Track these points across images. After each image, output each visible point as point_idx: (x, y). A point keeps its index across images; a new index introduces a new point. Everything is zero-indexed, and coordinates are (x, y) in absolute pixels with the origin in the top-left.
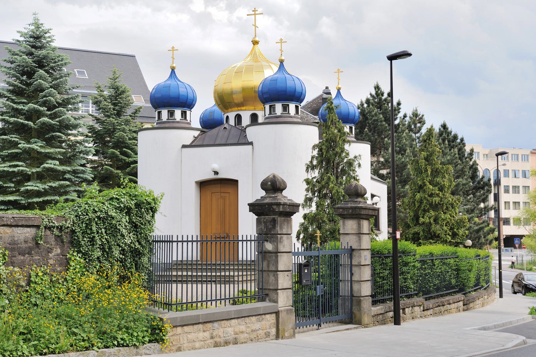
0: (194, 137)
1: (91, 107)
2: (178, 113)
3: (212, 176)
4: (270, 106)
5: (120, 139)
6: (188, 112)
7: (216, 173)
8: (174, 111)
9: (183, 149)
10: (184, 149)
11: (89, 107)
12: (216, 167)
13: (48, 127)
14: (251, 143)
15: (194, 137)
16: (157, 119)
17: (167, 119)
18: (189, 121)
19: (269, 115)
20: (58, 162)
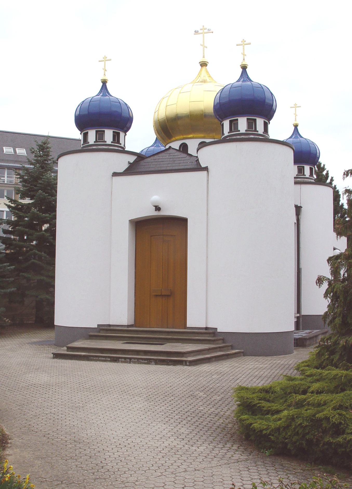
0: (129, 163)
1: (6, 177)
2: (109, 135)
3: (151, 213)
4: (231, 122)
5: (41, 196)
6: (122, 134)
7: (158, 208)
8: (104, 131)
10: (115, 178)
11: (4, 177)
14: (206, 169)
15: (129, 163)
16: (82, 143)
17: (95, 142)
18: (122, 145)
19: (229, 133)
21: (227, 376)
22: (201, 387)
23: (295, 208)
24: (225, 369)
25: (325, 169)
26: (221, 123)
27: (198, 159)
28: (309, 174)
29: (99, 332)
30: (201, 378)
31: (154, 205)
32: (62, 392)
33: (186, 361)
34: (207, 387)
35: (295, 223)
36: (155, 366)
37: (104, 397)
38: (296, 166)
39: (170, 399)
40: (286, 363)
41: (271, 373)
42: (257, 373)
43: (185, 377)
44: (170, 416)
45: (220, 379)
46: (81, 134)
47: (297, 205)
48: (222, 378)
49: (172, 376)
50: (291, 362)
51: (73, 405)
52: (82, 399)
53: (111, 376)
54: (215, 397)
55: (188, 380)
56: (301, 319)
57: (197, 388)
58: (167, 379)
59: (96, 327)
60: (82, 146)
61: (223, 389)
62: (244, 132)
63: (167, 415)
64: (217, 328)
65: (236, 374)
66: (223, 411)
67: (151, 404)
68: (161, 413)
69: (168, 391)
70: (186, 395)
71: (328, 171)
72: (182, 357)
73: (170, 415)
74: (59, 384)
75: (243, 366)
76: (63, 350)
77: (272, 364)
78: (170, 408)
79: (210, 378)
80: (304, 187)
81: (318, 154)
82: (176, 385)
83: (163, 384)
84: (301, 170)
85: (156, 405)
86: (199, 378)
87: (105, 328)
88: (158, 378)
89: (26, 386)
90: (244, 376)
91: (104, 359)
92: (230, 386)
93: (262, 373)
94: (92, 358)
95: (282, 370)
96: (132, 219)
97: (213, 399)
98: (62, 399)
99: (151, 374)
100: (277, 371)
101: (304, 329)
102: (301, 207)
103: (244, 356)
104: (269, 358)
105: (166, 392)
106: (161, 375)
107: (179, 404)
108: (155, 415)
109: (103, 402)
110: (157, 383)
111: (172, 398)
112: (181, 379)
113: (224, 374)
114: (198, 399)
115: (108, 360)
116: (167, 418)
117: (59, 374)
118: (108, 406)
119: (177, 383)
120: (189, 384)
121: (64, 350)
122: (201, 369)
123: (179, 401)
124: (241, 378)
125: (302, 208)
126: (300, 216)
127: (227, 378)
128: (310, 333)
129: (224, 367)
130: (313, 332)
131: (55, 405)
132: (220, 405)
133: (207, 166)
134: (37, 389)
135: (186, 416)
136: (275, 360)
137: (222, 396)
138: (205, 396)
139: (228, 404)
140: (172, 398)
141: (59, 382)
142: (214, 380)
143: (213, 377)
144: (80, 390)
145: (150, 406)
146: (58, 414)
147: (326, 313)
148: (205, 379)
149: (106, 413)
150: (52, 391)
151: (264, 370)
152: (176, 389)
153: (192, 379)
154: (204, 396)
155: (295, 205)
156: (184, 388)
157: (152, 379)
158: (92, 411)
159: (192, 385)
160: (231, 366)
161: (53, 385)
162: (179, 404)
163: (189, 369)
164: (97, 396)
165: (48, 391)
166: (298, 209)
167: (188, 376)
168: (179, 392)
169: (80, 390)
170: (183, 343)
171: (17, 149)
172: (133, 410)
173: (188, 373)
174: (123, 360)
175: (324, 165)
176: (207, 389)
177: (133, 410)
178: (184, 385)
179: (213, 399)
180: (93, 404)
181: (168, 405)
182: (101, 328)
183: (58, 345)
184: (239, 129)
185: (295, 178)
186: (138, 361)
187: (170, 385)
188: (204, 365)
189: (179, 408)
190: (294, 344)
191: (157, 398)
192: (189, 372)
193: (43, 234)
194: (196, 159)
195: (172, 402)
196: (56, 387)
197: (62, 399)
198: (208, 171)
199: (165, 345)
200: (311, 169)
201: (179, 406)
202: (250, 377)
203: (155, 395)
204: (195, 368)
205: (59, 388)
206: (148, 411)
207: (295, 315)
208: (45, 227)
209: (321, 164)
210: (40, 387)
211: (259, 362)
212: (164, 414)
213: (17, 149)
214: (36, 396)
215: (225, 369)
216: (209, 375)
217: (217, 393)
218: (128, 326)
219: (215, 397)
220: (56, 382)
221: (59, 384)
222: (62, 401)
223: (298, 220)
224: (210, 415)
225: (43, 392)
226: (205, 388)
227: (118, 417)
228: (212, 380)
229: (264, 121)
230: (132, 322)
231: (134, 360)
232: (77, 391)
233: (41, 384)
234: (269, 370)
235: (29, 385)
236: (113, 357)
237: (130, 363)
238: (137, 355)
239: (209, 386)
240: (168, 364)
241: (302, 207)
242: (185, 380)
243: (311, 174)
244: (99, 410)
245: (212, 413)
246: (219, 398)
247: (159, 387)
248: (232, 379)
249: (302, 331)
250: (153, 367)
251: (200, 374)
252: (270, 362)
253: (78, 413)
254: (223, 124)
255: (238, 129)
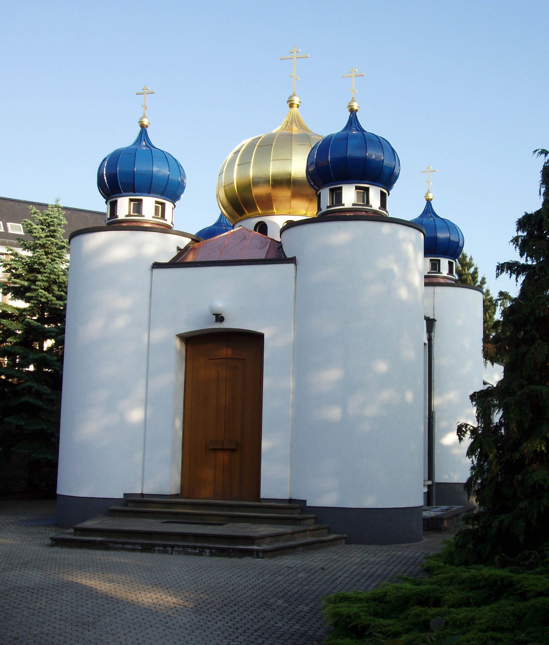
0: (178, 249)
4: (332, 191)
7: (219, 318)
9: (154, 270)
10: (156, 271)
12: (220, 305)
13: (37, 285)
14: (293, 260)
15: (178, 249)
20: (48, 341)
21: (320, 575)
22: (280, 592)
23: (425, 321)
24: (318, 563)
25: (473, 265)
26: (316, 193)
27: (282, 245)
28: (447, 272)
29: (126, 505)
30: (281, 577)
31: (214, 313)
32: (62, 599)
33: (257, 551)
34: (289, 591)
35: (425, 344)
36: (210, 558)
37: (129, 606)
38: (428, 259)
39: (231, 610)
40: (411, 555)
41: (388, 570)
42: (365, 570)
43: (255, 576)
44: (231, 637)
45: (310, 579)
46: (106, 202)
47: (429, 317)
48: (312, 577)
49: (236, 574)
50: (418, 554)
51: (78, 619)
52: (93, 610)
53: (142, 574)
54: (301, 607)
55: (261, 580)
56: (434, 488)
57: (274, 593)
58: (227, 579)
59: (122, 497)
60: (107, 222)
61: (314, 594)
62: (351, 206)
63: (226, 635)
64: (306, 501)
65: (334, 572)
66: (313, 629)
67: (202, 617)
68: (216, 633)
69: (229, 597)
70: (257, 603)
71: (476, 269)
72: (253, 544)
73: (230, 635)
74: (58, 586)
75: (345, 560)
76: (68, 534)
77: (389, 557)
78: (230, 624)
79: (294, 577)
80: (438, 289)
81: (461, 242)
82: (241, 588)
83: (221, 587)
84: (435, 266)
85: (209, 619)
86: (277, 577)
87: (136, 498)
88: (213, 577)
89: (4, 590)
90: (346, 575)
91: (132, 547)
92: (324, 590)
93: (374, 569)
94: (112, 545)
95: (405, 566)
96: (180, 334)
97: (297, 610)
98: (61, 611)
99: (204, 570)
100: (398, 568)
101: (439, 504)
102: (434, 320)
103: (347, 543)
104: (385, 548)
105: (226, 599)
106: (220, 572)
107: (245, 617)
108: (207, 636)
109: (126, 615)
110: (212, 585)
111: (235, 608)
112: (250, 579)
113: (316, 572)
114: (274, 610)
115: (137, 549)
116: (226, 640)
117: (60, 571)
118: (134, 622)
119: (244, 584)
120: (262, 587)
121: (70, 534)
122: (281, 563)
123: (245, 614)
124: (341, 578)
125: (436, 322)
126: (433, 334)
127: (320, 577)
128: (447, 510)
129: (315, 560)
130: (453, 509)
131: (49, 621)
132: (308, 620)
133: (295, 257)
134: (22, 595)
135: (255, 637)
136: (394, 551)
137: (312, 605)
138: (286, 605)
139: (320, 619)
140: (235, 608)
141: (58, 583)
142: (300, 580)
143: (299, 576)
144: (92, 596)
145: (199, 621)
146: (53, 635)
147: (470, 480)
148: (285, 579)
149: (130, 632)
150: (47, 598)
151: (377, 566)
152: (241, 595)
153: (267, 579)
154: (284, 605)
155: (425, 317)
156: (254, 593)
157: (205, 578)
158: (109, 629)
159: (265, 588)
160: (326, 558)
161: (48, 588)
162: (245, 617)
163: (261, 562)
164: (118, 605)
165: (40, 598)
166: (430, 323)
167: (260, 573)
168: (245, 599)
169: (92, 596)
170: (254, 523)
171: (9, 224)
172: (173, 627)
173: (260, 569)
174: (161, 548)
175: (471, 259)
176: (289, 594)
177: (173, 627)
178: (253, 587)
179: (297, 610)
180: (110, 618)
181: (228, 619)
182: (129, 498)
183: (59, 525)
184: (343, 203)
185: (426, 277)
186: (184, 549)
187: (232, 587)
188: (286, 557)
189: (245, 624)
190: (424, 526)
191: (212, 608)
192: (262, 568)
193: (44, 357)
194: (279, 246)
195: (235, 614)
196: (53, 592)
197: (61, 611)
198: (295, 264)
199: (226, 525)
200: (450, 264)
201: (245, 621)
202: (356, 576)
203: (209, 603)
204: (272, 561)
205: (57, 593)
206: (195, 629)
207: (424, 483)
208: (48, 343)
209: (466, 257)
210: (27, 592)
211: (370, 554)
212: (221, 633)
213: (9, 224)
214: (20, 606)
215: (318, 563)
216: (292, 572)
217: (304, 600)
218: (176, 496)
219: (301, 607)
220: (53, 584)
221: (58, 586)
222: (61, 613)
223: (430, 339)
224: (293, 635)
225: (31, 600)
226: (287, 593)
227: (150, 638)
228: (297, 580)
229: (381, 191)
230: (178, 491)
231: (178, 549)
232: (86, 598)
233: (29, 588)
234: (385, 566)
235: (10, 588)
236: (146, 545)
237: (172, 553)
238: (184, 540)
239: (292, 590)
240: (229, 556)
241: (436, 321)
242: (255, 581)
243: (451, 272)
244: (119, 627)
245: (295, 631)
246: (307, 609)
247: (215, 591)
248: (328, 580)
249: (436, 508)
250: (206, 560)
251: (279, 571)
252: (386, 554)
253: (86, 632)
254: (320, 193)
255: (342, 203)
